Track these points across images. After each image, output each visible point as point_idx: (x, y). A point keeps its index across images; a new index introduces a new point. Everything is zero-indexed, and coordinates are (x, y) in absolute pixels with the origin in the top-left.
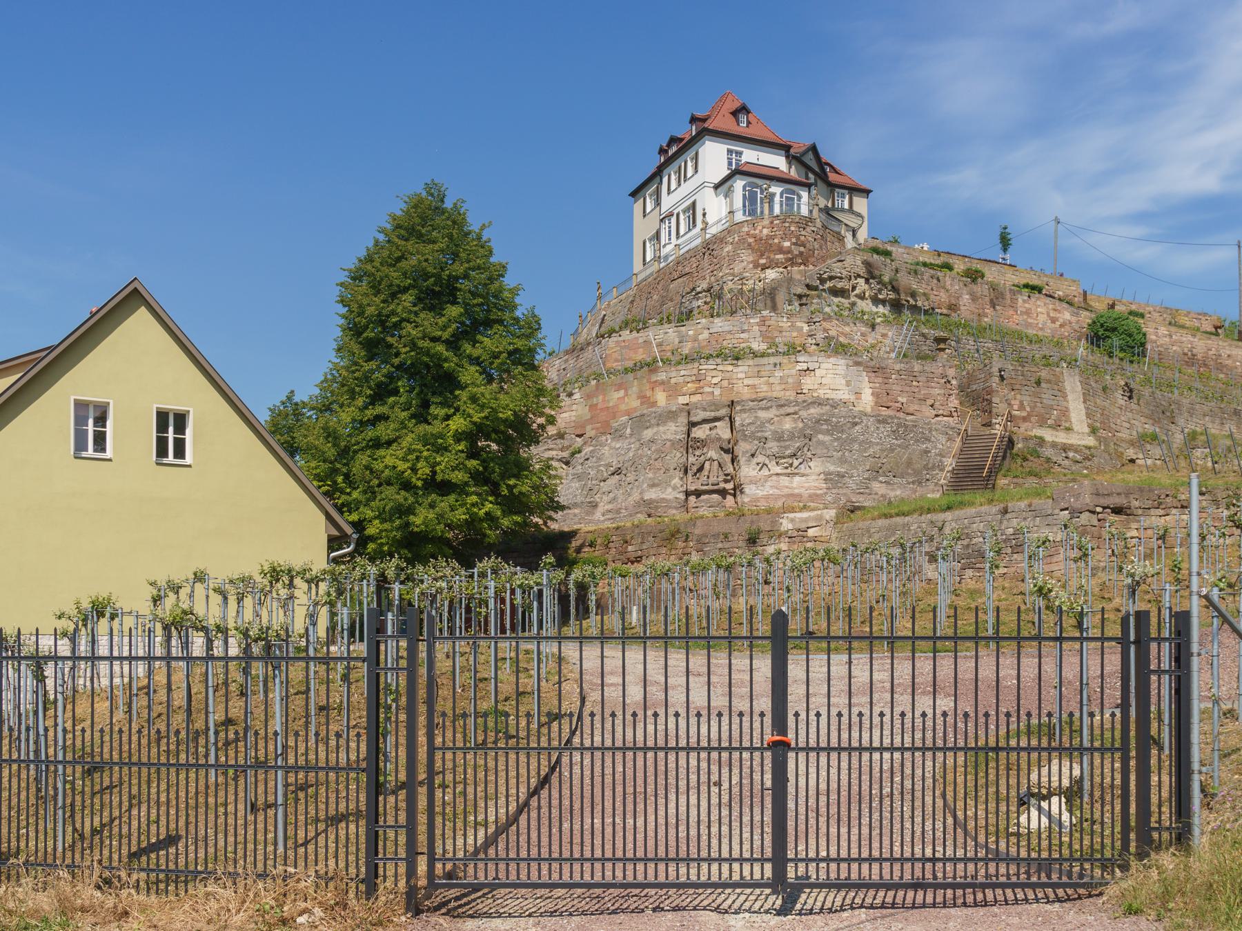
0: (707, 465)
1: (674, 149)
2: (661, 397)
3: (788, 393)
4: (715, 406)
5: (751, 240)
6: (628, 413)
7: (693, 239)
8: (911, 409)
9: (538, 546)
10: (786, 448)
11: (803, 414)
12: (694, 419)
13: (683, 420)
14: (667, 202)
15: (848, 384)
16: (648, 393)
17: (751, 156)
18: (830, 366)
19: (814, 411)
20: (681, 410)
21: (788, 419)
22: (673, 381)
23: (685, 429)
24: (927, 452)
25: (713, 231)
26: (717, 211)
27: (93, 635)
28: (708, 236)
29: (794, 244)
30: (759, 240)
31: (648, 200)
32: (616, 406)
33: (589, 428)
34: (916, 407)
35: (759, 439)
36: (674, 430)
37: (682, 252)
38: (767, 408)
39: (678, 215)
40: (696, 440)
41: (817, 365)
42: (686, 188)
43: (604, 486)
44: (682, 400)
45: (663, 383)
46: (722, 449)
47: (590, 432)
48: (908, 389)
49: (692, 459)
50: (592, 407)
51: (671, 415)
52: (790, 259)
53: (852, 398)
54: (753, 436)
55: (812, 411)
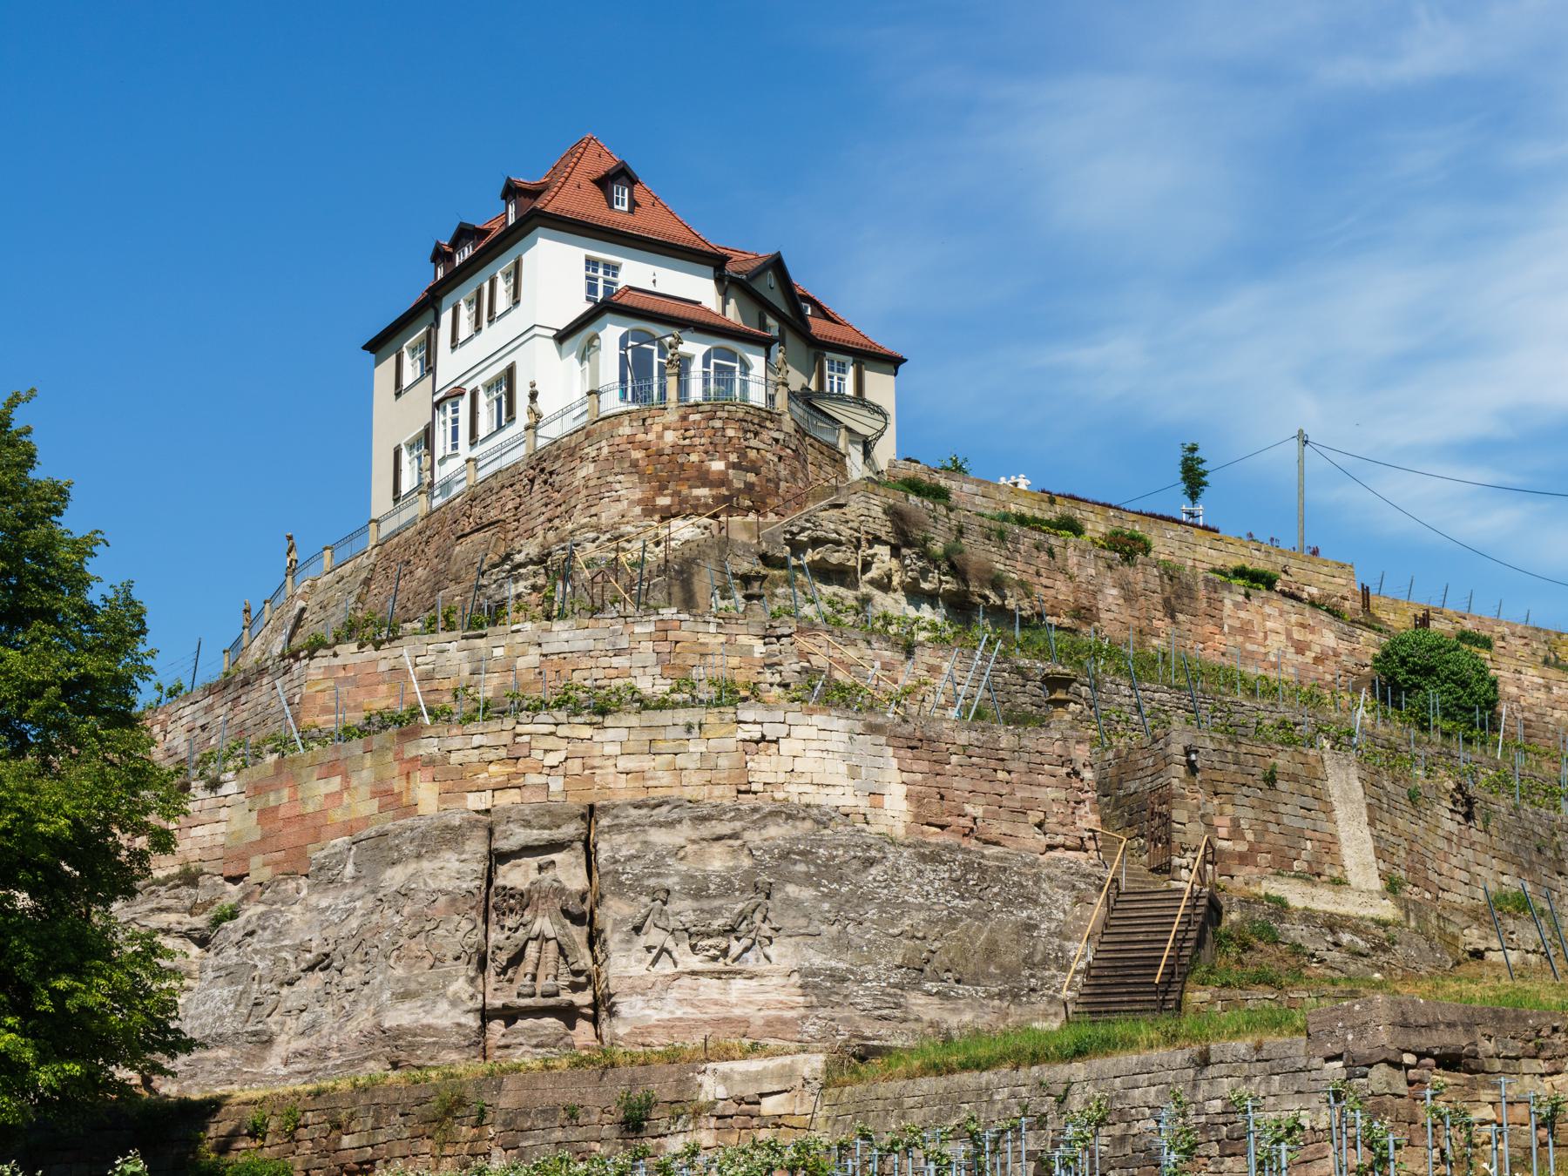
0: (532, 950)
1: (467, 252)
2: (426, 795)
3: (718, 791)
4: (555, 818)
5: (637, 454)
6: (348, 828)
7: (507, 449)
10: (714, 913)
12: (503, 845)
13: (476, 846)
14: (450, 365)
15: (853, 772)
17: (636, 273)
18: (812, 732)
19: (777, 832)
20: (473, 825)
21: (717, 848)
22: (455, 758)
23: (481, 867)
24: (1029, 927)
25: (552, 431)
26: (563, 389)
28: (541, 443)
29: (734, 466)
33: (256, 861)
35: (653, 893)
36: (456, 870)
37: (482, 475)
38: (671, 824)
39: (474, 394)
41: (782, 730)
42: (494, 337)
44: (475, 801)
45: (431, 762)
47: (259, 870)
48: (986, 787)
51: (450, 836)
52: (726, 499)
53: (863, 804)
54: (637, 886)
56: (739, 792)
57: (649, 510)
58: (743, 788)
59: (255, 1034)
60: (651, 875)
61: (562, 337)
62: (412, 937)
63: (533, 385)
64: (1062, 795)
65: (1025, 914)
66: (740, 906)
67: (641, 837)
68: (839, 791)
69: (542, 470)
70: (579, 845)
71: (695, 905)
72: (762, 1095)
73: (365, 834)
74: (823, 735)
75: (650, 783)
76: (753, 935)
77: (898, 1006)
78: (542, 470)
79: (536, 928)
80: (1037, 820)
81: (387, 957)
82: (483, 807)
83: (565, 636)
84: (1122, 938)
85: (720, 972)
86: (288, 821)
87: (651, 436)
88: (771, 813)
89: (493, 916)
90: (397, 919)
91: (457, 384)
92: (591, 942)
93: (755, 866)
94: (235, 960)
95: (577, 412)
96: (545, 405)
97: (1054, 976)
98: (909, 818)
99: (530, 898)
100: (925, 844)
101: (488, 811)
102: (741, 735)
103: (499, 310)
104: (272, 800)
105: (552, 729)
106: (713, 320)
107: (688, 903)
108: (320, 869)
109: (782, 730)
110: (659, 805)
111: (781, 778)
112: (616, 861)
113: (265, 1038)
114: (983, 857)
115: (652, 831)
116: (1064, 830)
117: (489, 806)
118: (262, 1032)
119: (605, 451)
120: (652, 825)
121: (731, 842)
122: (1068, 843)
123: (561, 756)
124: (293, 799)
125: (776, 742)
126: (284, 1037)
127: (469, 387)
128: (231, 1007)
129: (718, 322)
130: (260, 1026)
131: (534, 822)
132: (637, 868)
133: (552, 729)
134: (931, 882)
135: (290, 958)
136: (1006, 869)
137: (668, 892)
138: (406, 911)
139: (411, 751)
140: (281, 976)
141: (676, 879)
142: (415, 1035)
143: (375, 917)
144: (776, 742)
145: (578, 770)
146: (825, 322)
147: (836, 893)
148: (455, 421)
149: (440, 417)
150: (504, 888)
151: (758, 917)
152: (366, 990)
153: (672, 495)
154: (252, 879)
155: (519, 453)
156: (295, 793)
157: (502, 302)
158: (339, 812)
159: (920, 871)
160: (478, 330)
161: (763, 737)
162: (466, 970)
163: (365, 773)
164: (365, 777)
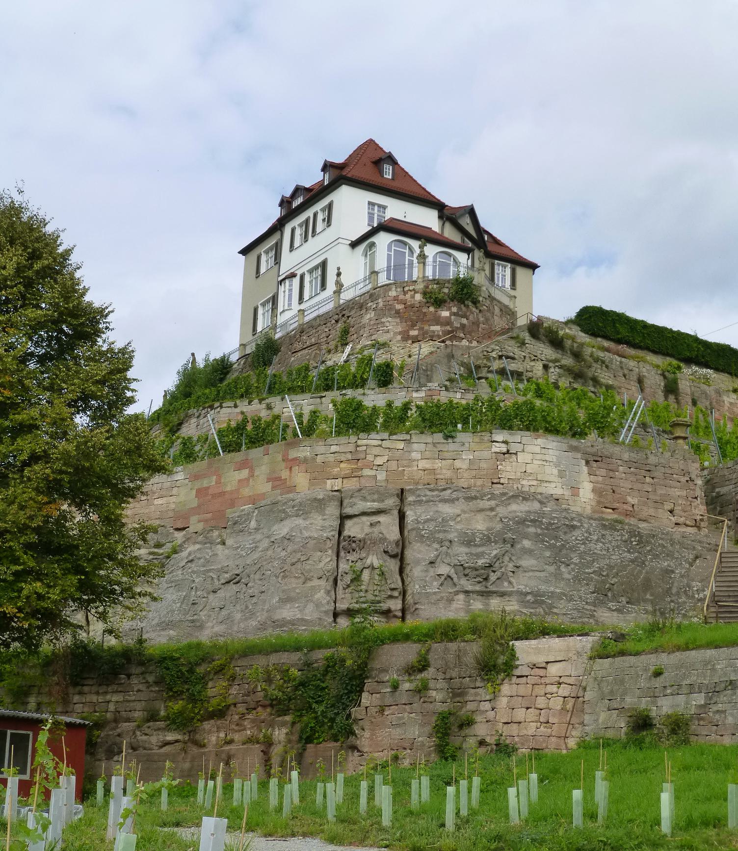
1: (299, 201)
2: (301, 479)
3: (479, 482)
5: (399, 307)
6: (253, 500)
7: (321, 303)
8: (644, 514)
10: (479, 556)
11: (502, 511)
12: (348, 511)
13: (333, 510)
14: (289, 261)
15: (561, 474)
16: (285, 474)
17: (398, 210)
18: (537, 449)
19: (519, 508)
20: (331, 499)
21: (480, 517)
22: (319, 459)
24: (668, 572)
25: (346, 296)
26: (353, 272)
28: (342, 302)
29: (454, 314)
30: (409, 307)
31: (264, 258)
32: (237, 491)
33: (194, 519)
34: (652, 512)
35: (441, 542)
36: (321, 525)
37: (307, 319)
38: (451, 501)
39: (302, 277)
41: (519, 447)
42: (314, 244)
43: (214, 600)
45: (305, 460)
47: (196, 525)
48: (639, 486)
49: (344, 566)
50: (200, 492)
51: (319, 504)
52: (449, 332)
53: (567, 493)
54: (431, 538)
55: (514, 507)
56: (493, 483)
57: (406, 337)
58: (495, 481)
59: (193, 621)
60: (440, 531)
61: (354, 245)
63: (339, 269)
64: (684, 493)
65: (666, 564)
66: (495, 552)
67: (435, 509)
68: (553, 485)
69: (343, 316)
70: (396, 512)
71: (466, 550)
72: (547, 663)
73: (263, 503)
74: (543, 451)
75: (438, 477)
76: (503, 570)
77: (592, 616)
78: (343, 316)
79: (369, 562)
80: (669, 508)
81: (277, 577)
83: (372, 397)
84: (731, 579)
85: (483, 592)
86: (214, 496)
87: (408, 296)
88: (513, 496)
89: (342, 554)
90: (283, 554)
91: (292, 271)
92: (401, 571)
93: (504, 528)
94: (181, 577)
95: (362, 285)
96: (346, 280)
97: (685, 603)
98: (594, 504)
99: (365, 543)
100: (603, 519)
102: (494, 449)
103: (318, 230)
104: (205, 483)
105: (380, 442)
106: (436, 237)
107: (464, 549)
108: (235, 524)
109: (519, 447)
110: (444, 490)
112: (419, 522)
113: (198, 624)
114: (639, 528)
115: (440, 505)
116: (685, 514)
118: (198, 620)
119: (381, 305)
120: (441, 501)
121: (488, 513)
122: (688, 522)
123: (386, 458)
124: (218, 482)
125: (516, 454)
126: (210, 624)
127: (299, 273)
128: (178, 605)
129: (439, 238)
130: (195, 617)
131: (368, 498)
132: (431, 526)
133: (380, 442)
134: (610, 542)
136: (654, 536)
138: (290, 549)
139: (293, 454)
140: (211, 588)
141: (456, 534)
142: (293, 625)
143: (270, 553)
144: (516, 454)
145: (395, 468)
146: (497, 246)
147: (554, 546)
148: (290, 290)
149: (282, 289)
150: (349, 537)
151: (506, 558)
152: (263, 596)
153: (419, 330)
154: (192, 529)
155: (330, 306)
157: (320, 226)
158: (247, 490)
159: (603, 535)
160: (306, 239)
161: (508, 451)
162: (325, 584)
163: (263, 467)
164: (262, 471)
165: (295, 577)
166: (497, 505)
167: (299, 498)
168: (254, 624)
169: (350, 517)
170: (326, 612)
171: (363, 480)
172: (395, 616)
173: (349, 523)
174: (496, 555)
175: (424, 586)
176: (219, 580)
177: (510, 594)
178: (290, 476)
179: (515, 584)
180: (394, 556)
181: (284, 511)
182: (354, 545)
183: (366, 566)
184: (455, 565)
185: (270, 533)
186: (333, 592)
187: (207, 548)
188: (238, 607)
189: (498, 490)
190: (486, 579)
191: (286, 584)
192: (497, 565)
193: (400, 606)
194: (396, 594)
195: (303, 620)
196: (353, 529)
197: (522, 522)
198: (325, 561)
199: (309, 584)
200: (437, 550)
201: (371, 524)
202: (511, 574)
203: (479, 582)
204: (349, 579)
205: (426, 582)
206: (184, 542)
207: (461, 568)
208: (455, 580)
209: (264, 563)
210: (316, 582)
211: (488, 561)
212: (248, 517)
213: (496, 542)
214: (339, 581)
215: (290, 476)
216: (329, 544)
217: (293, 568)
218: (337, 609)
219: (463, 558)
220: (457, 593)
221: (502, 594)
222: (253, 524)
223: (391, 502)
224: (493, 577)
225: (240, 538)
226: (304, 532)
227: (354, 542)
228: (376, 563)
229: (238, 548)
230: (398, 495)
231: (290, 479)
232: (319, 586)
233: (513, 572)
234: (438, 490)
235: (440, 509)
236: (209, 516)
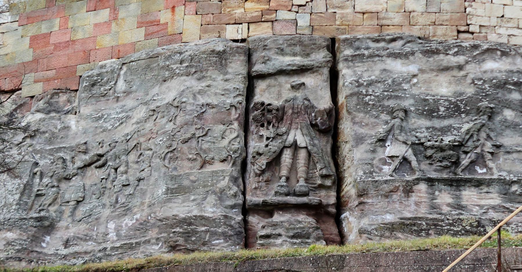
0: (287, 157)
3: (440, 31)
4: (306, 46)
6: (116, 52)
9: (51, 224)
10: (445, 131)
11: (473, 70)
12: (258, 68)
13: (237, 67)
16: (165, 17)
19: (494, 66)
23: (242, 87)
27: (309, 160)
35: (391, 112)
36: (224, 87)
40: (265, 108)
44: (232, 32)
46: (314, 126)
49: (255, 145)
51: (221, 58)
54: (379, 106)
56: (459, 32)
58: (462, 29)
59: (39, 219)
60: (390, 98)
62: (185, 142)
66: (466, 127)
70: (326, 71)
71: (428, 123)
75: (384, 22)
76: (478, 150)
79: (290, 139)
82: (239, 37)
86: (57, 46)
88: (488, 50)
89: (253, 128)
90: (170, 126)
94: (18, 158)
101: (243, 41)
107: (424, 123)
108: (93, 85)
110: (394, 40)
111: (494, 21)
112: (360, 85)
113: (47, 223)
117: (245, 36)
120: (390, 55)
121: (455, 73)
124: (63, 27)
128: (17, 197)
131: (288, 50)
132: (379, 89)
135: (68, 158)
137: (406, 112)
141: (412, 101)
142: (190, 224)
143: (149, 125)
150: (263, 104)
151: (483, 135)
154: (25, 92)
156: (66, 23)
165: (189, 159)
166: (467, 62)
167: (190, 49)
168: (130, 223)
169: (262, 76)
170: (233, 207)
171: (278, 26)
172: (328, 214)
173: (261, 86)
174: (468, 131)
175: (371, 173)
176: (73, 163)
177: (489, 183)
178: (173, 20)
179: (495, 171)
180: (323, 132)
181: (167, 68)
182: (270, 116)
183: (287, 144)
184: (413, 144)
185: (149, 98)
186: (241, 180)
187: (53, 118)
188: (105, 200)
189: (467, 41)
190: (457, 163)
191: (175, 169)
192: (470, 143)
193: (333, 200)
194: (328, 183)
195: (202, 218)
196: (264, 94)
197: (502, 85)
198: (227, 137)
199: (209, 169)
200: (387, 123)
201: (293, 87)
202: (489, 156)
203: (446, 167)
204: (265, 162)
205: (372, 166)
206: (15, 110)
207: (418, 147)
208: (414, 164)
209: (142, 140)
210: (218, 166)
211: (457, 138)
212: (115, 74)
213: (467, 113)
214: (249, 166)
215: (173, 20)
216: (234, 114)
217: (185, 147)
218: (248, 202)
219: (423, 135)
220: (418, 181)
221: (479, 184)
222: (121, 85)
223: (321, 56)
224: (465, 161)
225: (102, 105)
226: (199, 96)
227: (270, 111)
228: (302, 141)
229: (100, 118)
230: (328, 48)
231: (173, 23)
232: (223, 171)
233: (492, 154)
234: (384, 40)
235: (388, 67)
236: (51, 74)
